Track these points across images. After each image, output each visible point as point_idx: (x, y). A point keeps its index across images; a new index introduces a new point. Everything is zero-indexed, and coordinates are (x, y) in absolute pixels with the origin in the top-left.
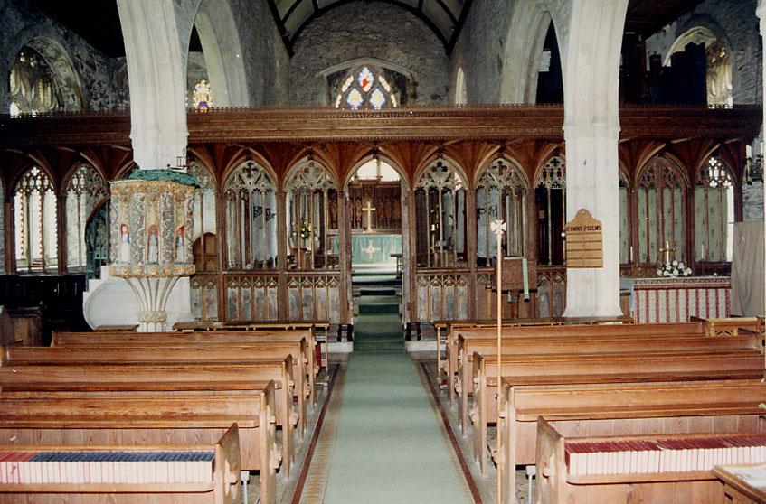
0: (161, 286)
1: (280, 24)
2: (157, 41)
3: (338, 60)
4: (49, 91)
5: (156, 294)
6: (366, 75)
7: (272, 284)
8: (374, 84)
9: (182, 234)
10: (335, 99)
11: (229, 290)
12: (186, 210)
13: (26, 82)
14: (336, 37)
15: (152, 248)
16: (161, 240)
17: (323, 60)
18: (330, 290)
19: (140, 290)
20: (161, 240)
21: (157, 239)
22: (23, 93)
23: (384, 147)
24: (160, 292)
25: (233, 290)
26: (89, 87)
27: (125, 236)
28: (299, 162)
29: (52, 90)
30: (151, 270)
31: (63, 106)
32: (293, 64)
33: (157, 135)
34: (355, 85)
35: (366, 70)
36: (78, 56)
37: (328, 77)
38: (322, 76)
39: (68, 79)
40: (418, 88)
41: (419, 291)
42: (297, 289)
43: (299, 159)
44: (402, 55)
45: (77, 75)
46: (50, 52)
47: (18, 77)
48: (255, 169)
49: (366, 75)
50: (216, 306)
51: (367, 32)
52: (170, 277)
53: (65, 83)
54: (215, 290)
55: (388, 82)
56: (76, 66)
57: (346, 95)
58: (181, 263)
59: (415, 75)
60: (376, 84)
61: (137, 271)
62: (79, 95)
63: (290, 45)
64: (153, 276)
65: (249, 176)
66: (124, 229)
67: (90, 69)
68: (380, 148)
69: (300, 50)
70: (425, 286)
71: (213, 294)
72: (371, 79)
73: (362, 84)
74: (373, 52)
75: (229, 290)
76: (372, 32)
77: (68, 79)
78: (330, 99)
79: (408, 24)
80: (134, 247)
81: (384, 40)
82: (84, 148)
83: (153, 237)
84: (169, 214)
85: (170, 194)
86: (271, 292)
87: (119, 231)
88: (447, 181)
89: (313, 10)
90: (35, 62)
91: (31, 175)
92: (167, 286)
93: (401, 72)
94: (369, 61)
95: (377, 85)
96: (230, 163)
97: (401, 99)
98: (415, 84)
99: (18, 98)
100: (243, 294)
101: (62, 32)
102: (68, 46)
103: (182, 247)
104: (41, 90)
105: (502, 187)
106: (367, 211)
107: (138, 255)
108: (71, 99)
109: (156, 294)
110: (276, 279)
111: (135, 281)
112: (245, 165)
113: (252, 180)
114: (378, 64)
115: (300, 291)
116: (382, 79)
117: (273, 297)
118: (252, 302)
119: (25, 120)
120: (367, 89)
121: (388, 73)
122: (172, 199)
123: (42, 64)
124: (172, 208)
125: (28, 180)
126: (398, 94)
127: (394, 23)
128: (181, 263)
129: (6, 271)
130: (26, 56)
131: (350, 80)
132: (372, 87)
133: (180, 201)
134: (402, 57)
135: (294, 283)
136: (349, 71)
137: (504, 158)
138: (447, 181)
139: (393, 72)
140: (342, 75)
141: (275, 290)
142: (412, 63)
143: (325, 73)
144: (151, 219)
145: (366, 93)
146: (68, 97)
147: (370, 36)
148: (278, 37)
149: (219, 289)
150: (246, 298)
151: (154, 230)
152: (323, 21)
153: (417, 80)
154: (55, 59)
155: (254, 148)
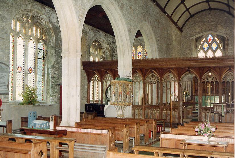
0: (122, 108)
1: (175, 24)
2: (124, 43)
3: (199, 33)
4: (101, 51)
5: (121, 110)
6: (210, 37)
7: (158, 109)
8: (213, 40)
9: (128, 94)
10: (198, 47)
11: (146, 111)
12: (129, 88)
13: (95, 49)
14: (198, 24)
15: (120, 98)
16: (122, 96)
17: (194, 33)
18: (175, 112)
19: (117, 108)
20: (122, 96)
21: (121, 95)
22: (94, 53)
23: (191, 69)
24: (122, 109)
25: (147, 111)
26: (112, 49)
27: (114, 94)
28: (167, 74)
29: (102, 51)
30: (119, 103)
31: (105, 55)
32: (182, 35)
33: (125, 69)
34: (206, 41)
35: (210, 36)
36: (109, 40)
37: (196, 39)
38: (193, 39)
39: (106, 48)
40: (229, 42)
41: (203, 114)
42: (165, 112)
43: (167, 73)
44: (223, 29)
45: (109, 46)
46: (101, 40)
47: (93, 48)
48: (154, 75)
49: (210, 37)
50: (142, 115)
51: (210, 22)
52: (125, 105)
53: (106, 49)
54: (142, 111)
55: (218, 40)
56: (109, 44)
57: (202, 45)
58: (127, 102)
59: (228, 36)
60: (214, 40)
61: (116, 104)
62: (109, 52)
63: (181, 30)
64: (120, 105)
65: (153, 78)
66: (114, 92)
67: (113, 44)
68: (190, 69)
69: (185, 30)
70: (204, 112)
71: (142, 112)
72: (212, 38)
73: (208, 40)
74: (212, 30)
75: (146, 111)
76: (212, 22)
77: (106, 48)
78: (196, 46)
79: (225, 18)
80: (116, 97)
81: (216, 24)
82: (108, 70)
83: (120, 95)
84: (125, 89)
85: (125, 84)
86: (158, 112)
87: (112, 93)
88: (212, 79)
89: (190, 16)
90: (97, 43)
91: (95, 77)
92: (124, 108)
93: (223, 35)
94: (212, 32)
95: (214, 41)
96: (147, 74)
97: (223, 45)
98: (228, 40)
99: (93, 54)
100: (150, 112)
101: (105, 35)
102: (106, 38)
103: (128, 98)
104: (99, 51)
105: (231, 82)
106: (208, 87)
107: (117, 100)
108: (107, 53)
109: (121, 110)
110: (159, 108)
111: (116, 106)
112: (151, 74)
113: (153, 79)
114: (215, 34)
115: (166, 112)
116: (216, 38)
117: (158, 114)
118: (152, 115)
119: (94, 62)
120: (210, 42)
121: (218, 37)
122: (125, 85)
123: (99, 44)
124: (125, 87)
125: (94, 78)
126: (222, 44)
127: (220, 18)
128: (127, 102)
129: (88, 102)
130: (95, 42)
131: (204, 39)
132: (212, 42)
133: (128, 86)
134: (223, 30)
135: (164, 110)
136: (204, 36)
137: (231, 72)
138: (212, 79)
139: (220, 36)
140: (201, 38)
141: (159, 111)
142: (227, 32)
143: (194, 38)
144: (120, 90)
145: (210, 44)
146: (107, 52)
147: (211, 23)
148: (174, 27)
149: (143, 110)
150: (151, 113)
151: (121, 93)
152: (193, 19)
153: (229, 38)
154: (103, 42)
155: (153, 70)
